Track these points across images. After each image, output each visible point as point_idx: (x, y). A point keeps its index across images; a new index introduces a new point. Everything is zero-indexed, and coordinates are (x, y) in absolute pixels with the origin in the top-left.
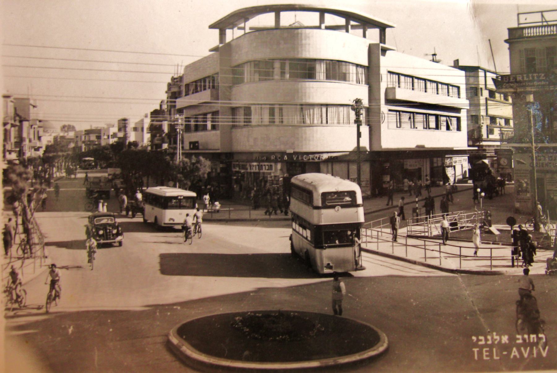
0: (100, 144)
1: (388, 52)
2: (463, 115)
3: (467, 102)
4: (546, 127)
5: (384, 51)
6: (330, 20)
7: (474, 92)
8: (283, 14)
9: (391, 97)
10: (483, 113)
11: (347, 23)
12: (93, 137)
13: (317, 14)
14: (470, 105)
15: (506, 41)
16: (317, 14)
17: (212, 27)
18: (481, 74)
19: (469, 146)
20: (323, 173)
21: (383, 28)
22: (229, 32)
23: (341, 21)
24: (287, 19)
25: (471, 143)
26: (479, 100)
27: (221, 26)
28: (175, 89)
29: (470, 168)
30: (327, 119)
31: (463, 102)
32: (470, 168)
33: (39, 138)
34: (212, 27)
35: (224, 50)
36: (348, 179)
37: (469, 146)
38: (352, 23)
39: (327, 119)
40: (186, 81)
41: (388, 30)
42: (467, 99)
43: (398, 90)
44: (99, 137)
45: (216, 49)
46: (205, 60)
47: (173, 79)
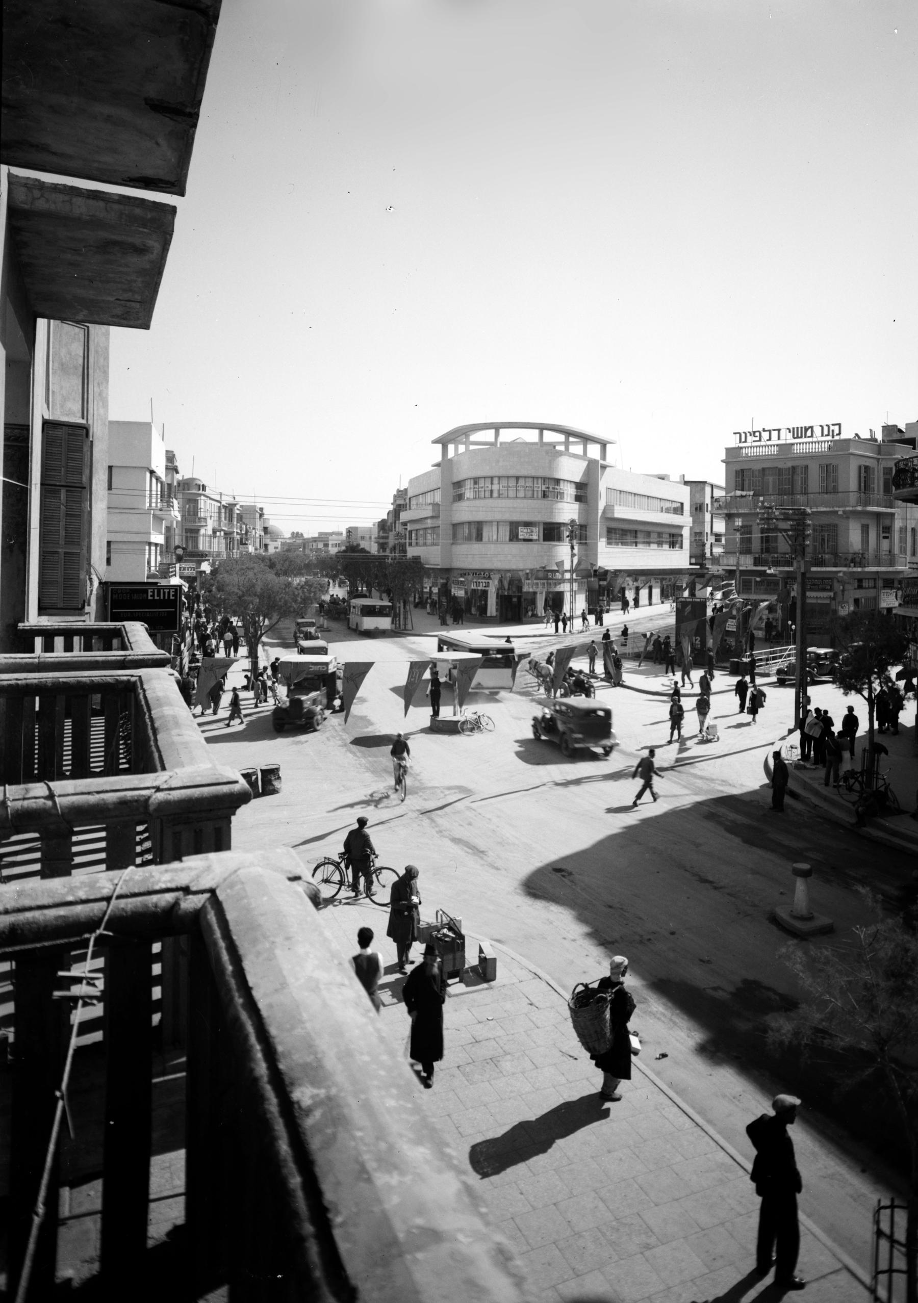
1: (608, 469)
2: (686, 533)
3: (691, 519)
4: (304, 629)
5: (604, 467)
6: (549, 436)
7: (698, 508)
8: (501, 431)
9: (609, 516)
10: (707, 529)
12: (321, 546)
13: (537, 432)
14: (694, 522)
15: (723, 461)
16: (537, 432)
17: (436, 442)
18: (708, 489)
19: (691, 564)
20: (900, 615)
21: (604, 445)
22: (451, 447)
23: (561, 438)
25: (693, 561)
27: (443, 442)
28: (401, 502)
30: (535, 636)
31: (685, 521)
34: (436, 442)
35: (445, 465)
38: (571, 439)
39: (535, 636)
41: (608, 446)
42: (691, 515)
43: (617, 508)
44: (326, 545)
45: (438, 465)
47: (399, 491)
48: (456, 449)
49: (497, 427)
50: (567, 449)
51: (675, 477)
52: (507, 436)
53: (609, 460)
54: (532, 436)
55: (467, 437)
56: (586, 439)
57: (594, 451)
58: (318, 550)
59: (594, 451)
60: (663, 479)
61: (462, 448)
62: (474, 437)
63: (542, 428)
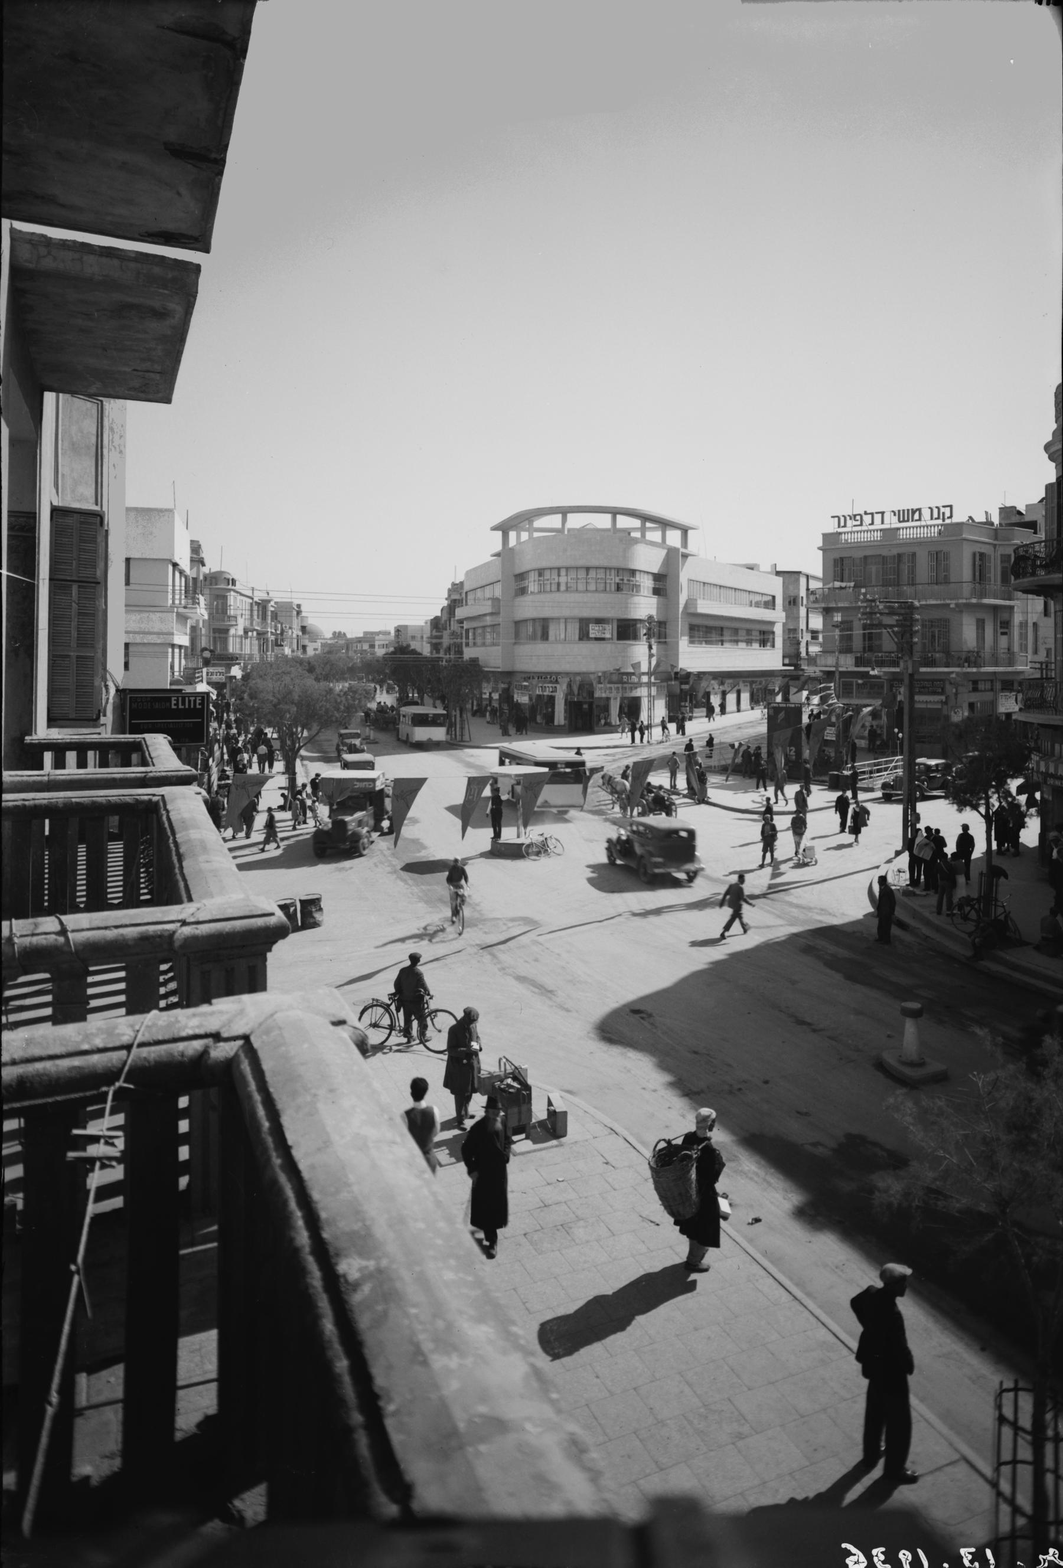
0: (373, 654)
3: (784, 614)
5: (685, 556)
6: (623, 522)
7: (792, 602)
8: (569, 516)
9: (692, 611)
10: (802, 625)
11: (643, 525)
12: (366, 647)
13: (609, 516)
15: (819, 548)
16: (609, 516)
17: (495, 529)
18: (803, 580)
19: (784, 665)
21: (685, 531)
22: (512, 535)
23: (637, 523)
24: (623, 522)
25: (787, 661)
26: (798, 613)
29: (94, 1482)
31: (778, 616)
32: (94, 1482)
33: (304, 647)
35: (505, 555)
36: (883, 557)
37: (784, 665)
38: (648, 525)
40: (466, 588)
41: (690, 532)
42: (784, 610)
43: (700, 602)
44: (372, 646)
45: (498, 555)
46: (487, 565)
47: (454, 584)
48: (518, 537)
49: (564, 512)
50: (643, 536)
51: (766, 567)
52: (575, 521)
53: (692, 548)
54: (603, 521)
55: (531, 522)
56: (664, 524)
57: (674, 538)
58: (363, 652)
59: (674, 538)
60: (752, 569)
61: (525, 536)
62: (539, 523)
63: (615, 512)
